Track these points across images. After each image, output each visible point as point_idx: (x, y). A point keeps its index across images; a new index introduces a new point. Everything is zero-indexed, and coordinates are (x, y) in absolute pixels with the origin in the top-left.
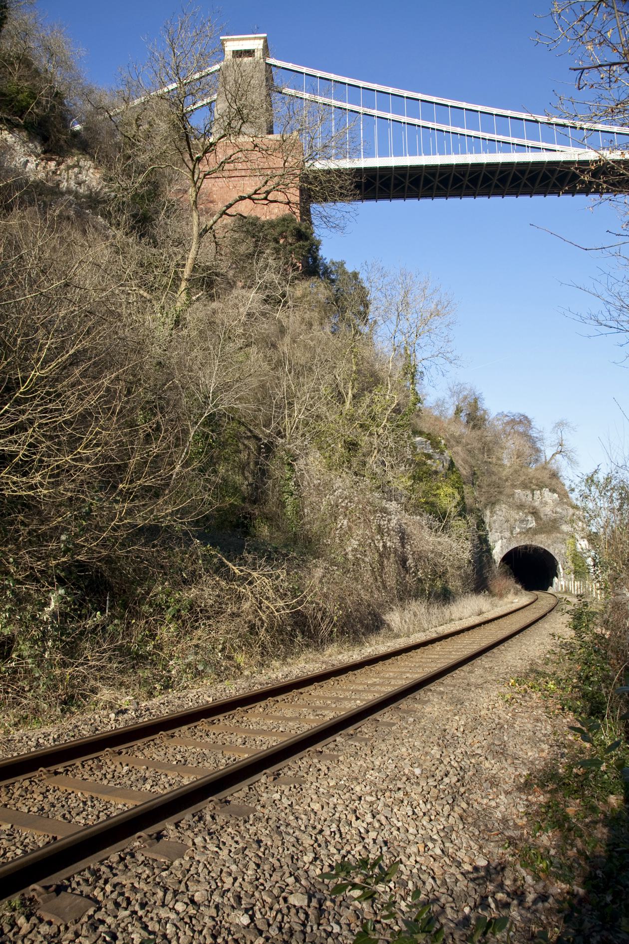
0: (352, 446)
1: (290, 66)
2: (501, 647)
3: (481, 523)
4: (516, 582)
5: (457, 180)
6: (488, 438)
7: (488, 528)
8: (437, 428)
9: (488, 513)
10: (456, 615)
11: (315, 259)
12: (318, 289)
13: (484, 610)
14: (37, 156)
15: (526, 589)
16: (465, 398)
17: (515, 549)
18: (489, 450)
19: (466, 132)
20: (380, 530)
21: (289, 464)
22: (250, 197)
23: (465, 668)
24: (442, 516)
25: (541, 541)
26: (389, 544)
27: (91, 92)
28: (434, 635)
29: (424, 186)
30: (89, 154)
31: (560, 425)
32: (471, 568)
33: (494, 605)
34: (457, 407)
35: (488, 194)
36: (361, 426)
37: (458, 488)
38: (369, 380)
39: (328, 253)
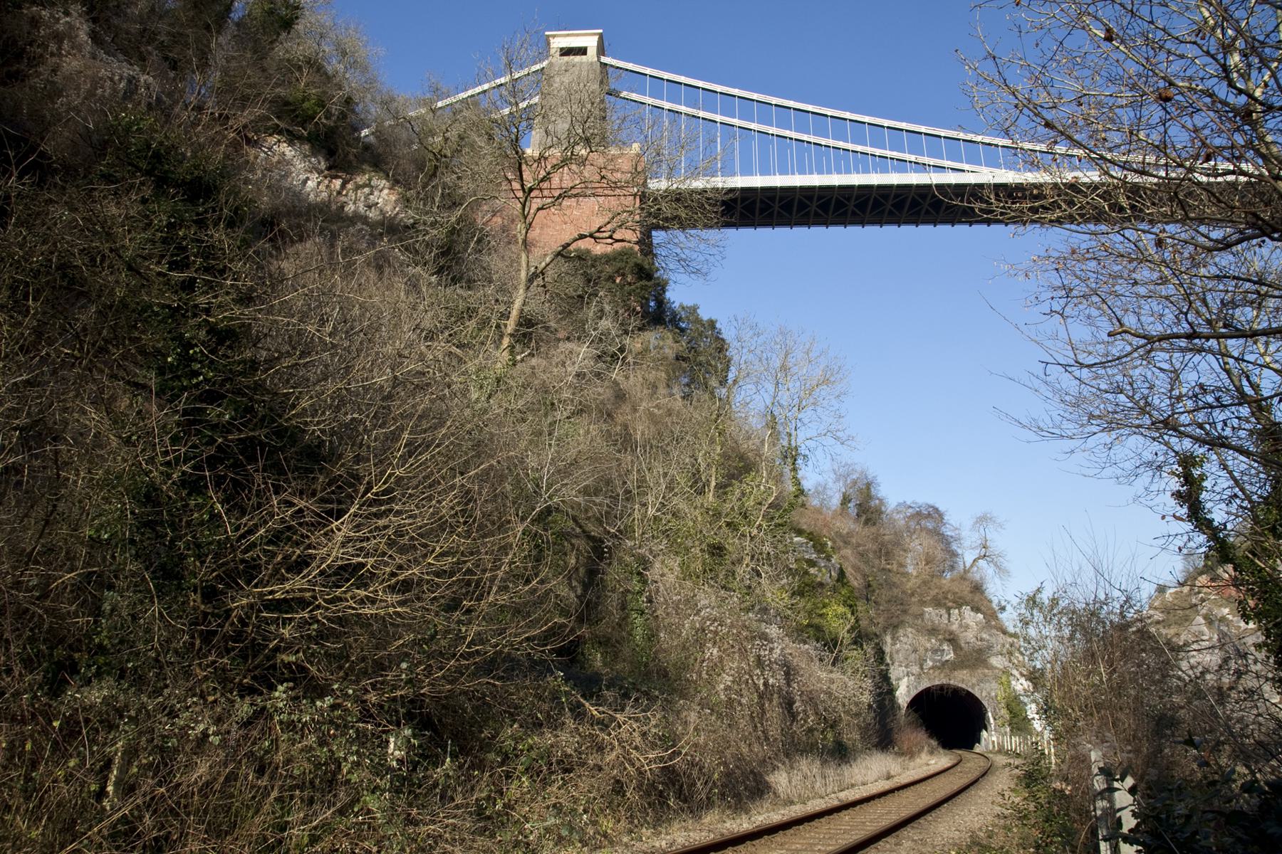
0: (717, 550)
1: (630, 66)
2: (929, 817)
3: (880, 655)
4: (931, 736)
5: (840, 205)
6: (886, 538)
7: (888, 661)
8: (820, 523)
9: (888, 639)
10: (859, 778)
11: (661, 302)
12: (658, 341)
13: (892, 773)
14: (320, 172)
15: (944, 747)
16: (855, 482)
17: (927, 690)
18: (887, 553)
19: (850, 146)
20: (759, 662)
21: (639, 574)
22: (591, 236)
23: (891, 839)
24: (832, 643)
25: (962, 680)
26: (771, 681)
27: (393, 100)
28: (836, 803)
29: (798, 211)
30: (381, 170)
31: (983, 520)
32: (873, 714)
33: (905, 768)
34: (844, 495)
35: (881, 223)
36: (728, 524)
37: (851, 606)
38: (739, 466)
39: (677, 296)
